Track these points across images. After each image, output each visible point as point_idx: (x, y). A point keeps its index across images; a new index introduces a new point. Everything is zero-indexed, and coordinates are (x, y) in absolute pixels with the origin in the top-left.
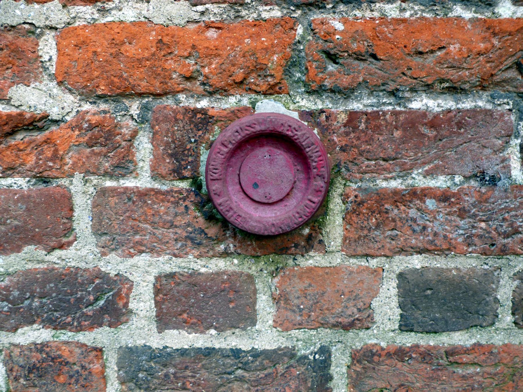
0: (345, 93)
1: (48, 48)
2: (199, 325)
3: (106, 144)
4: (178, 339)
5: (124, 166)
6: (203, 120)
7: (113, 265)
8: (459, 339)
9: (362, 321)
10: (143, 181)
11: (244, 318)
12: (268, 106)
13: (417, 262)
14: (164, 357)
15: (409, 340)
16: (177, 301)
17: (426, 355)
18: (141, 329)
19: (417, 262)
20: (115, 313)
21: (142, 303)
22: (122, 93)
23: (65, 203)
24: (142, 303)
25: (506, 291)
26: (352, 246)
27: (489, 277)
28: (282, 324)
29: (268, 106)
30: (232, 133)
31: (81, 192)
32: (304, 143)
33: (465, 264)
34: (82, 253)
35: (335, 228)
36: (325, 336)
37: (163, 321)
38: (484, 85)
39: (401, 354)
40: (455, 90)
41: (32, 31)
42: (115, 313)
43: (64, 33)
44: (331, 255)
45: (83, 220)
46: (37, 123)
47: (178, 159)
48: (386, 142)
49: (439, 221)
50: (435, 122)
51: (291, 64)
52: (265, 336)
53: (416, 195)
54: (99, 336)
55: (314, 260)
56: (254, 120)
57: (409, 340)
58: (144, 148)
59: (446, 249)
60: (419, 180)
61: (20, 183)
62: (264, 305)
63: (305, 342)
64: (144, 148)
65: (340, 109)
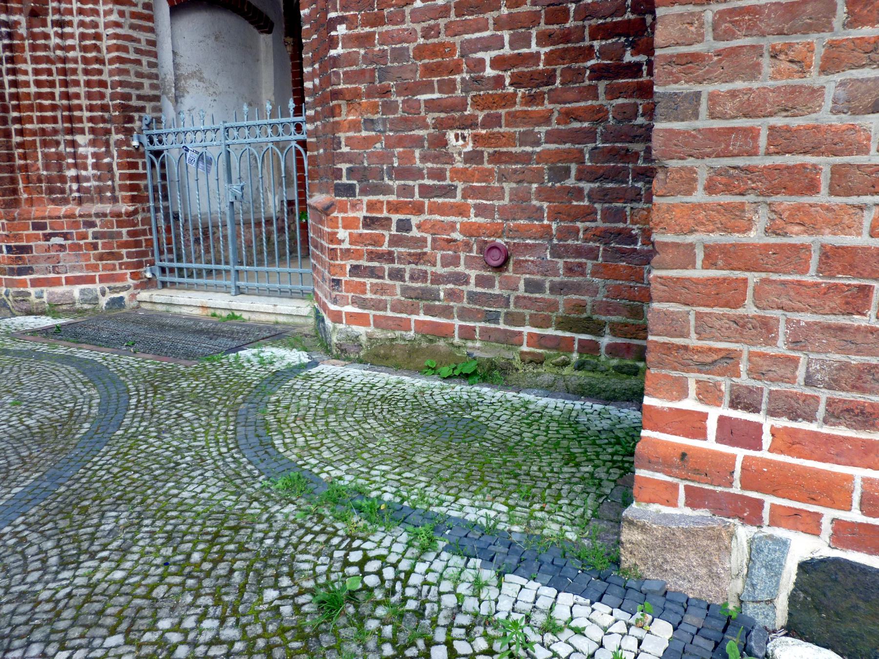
0: (514, 238)
1: (458, 226)
2: (484, 287)
3: (468, 246)
4: (479, 290)
5: (471, 251)
6: (486, 242)
7: (467, 272)
8: (537, 295)
9: (516, 289)
10: (474, 254)
11: (492, 286)
12: (498, 241)
13: (528, 276)
14: (476, 294)
15: (526, 294)
16: (481, 281)
17: (530, 299)
18: (472, 287)
19: (528, 276)
20: (467, 283)
21: (472, 281)
22: (471, 236)
23: (459, 257)
24: (472, 281)
25: (547, 285)
26: (515, 271)
27: (544, 281)
28: (501, 288)
29: (498, 241)
30: (488, 246)
31: (462, 255)
32: (640, 473)
33: (538, 277)
34: (461, 269)
35: (511, 267)
36: (509, 292)
37: (477, 285)
38: (541, 237)
39: (525, 298)
40: (535, 239)
41: (455, 223)
42: (467, 283)
43: (461, 223)
44: (510, 273)
45: (462, 262)
46: (455, 241)
47: (481, 250)
48: (521, 249)
49: (532, 267)
50: (530, 245)
51: (503, 232)
52: (496, 291)
53: (527, 261)
54: (463, 288)
55: (506, 274)
56: (254, 103)
57: (526, 294)
58: (475, 247)
59: (533, 274)
60: (527, 258)
61: (451, 253)
62: (497, 283)
63: (505, 293)
64: (475, 247)
65: (512, 242)
